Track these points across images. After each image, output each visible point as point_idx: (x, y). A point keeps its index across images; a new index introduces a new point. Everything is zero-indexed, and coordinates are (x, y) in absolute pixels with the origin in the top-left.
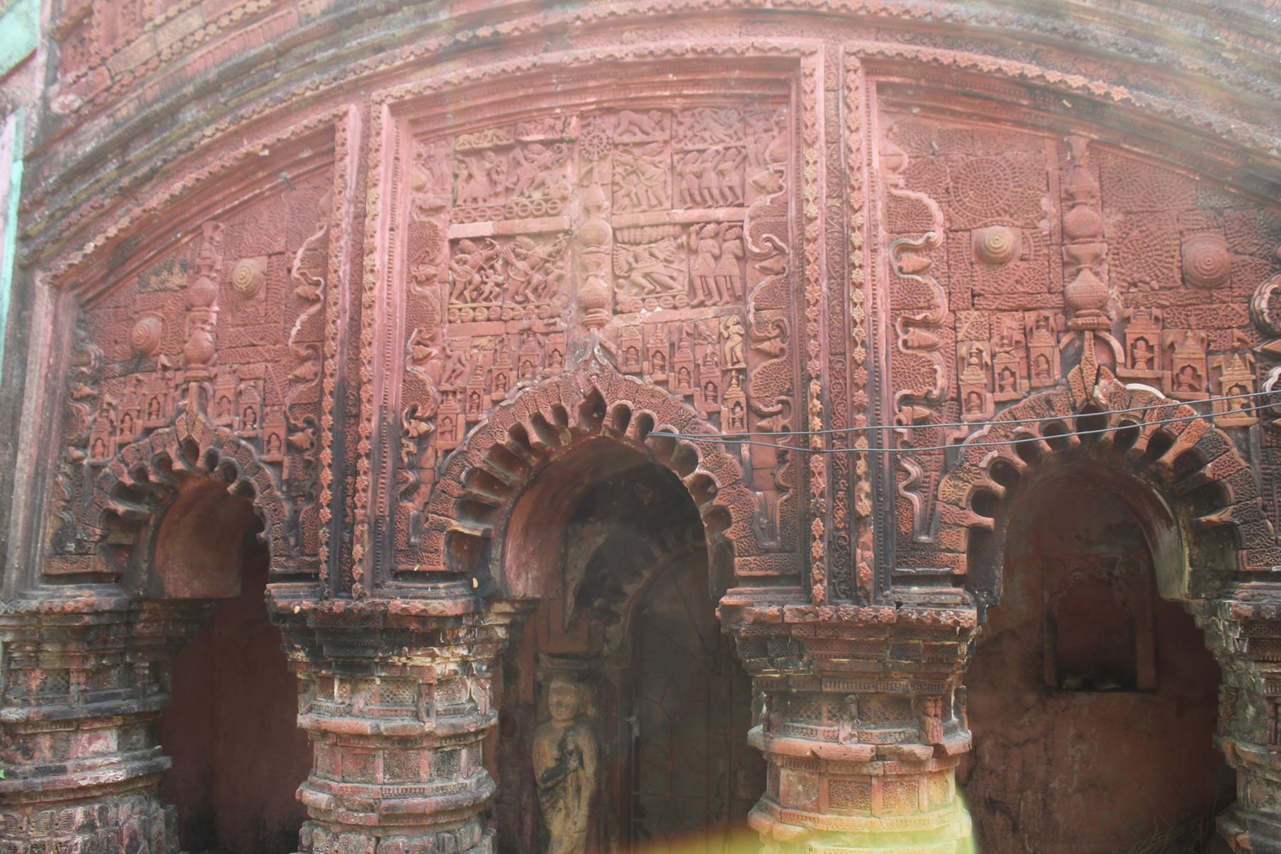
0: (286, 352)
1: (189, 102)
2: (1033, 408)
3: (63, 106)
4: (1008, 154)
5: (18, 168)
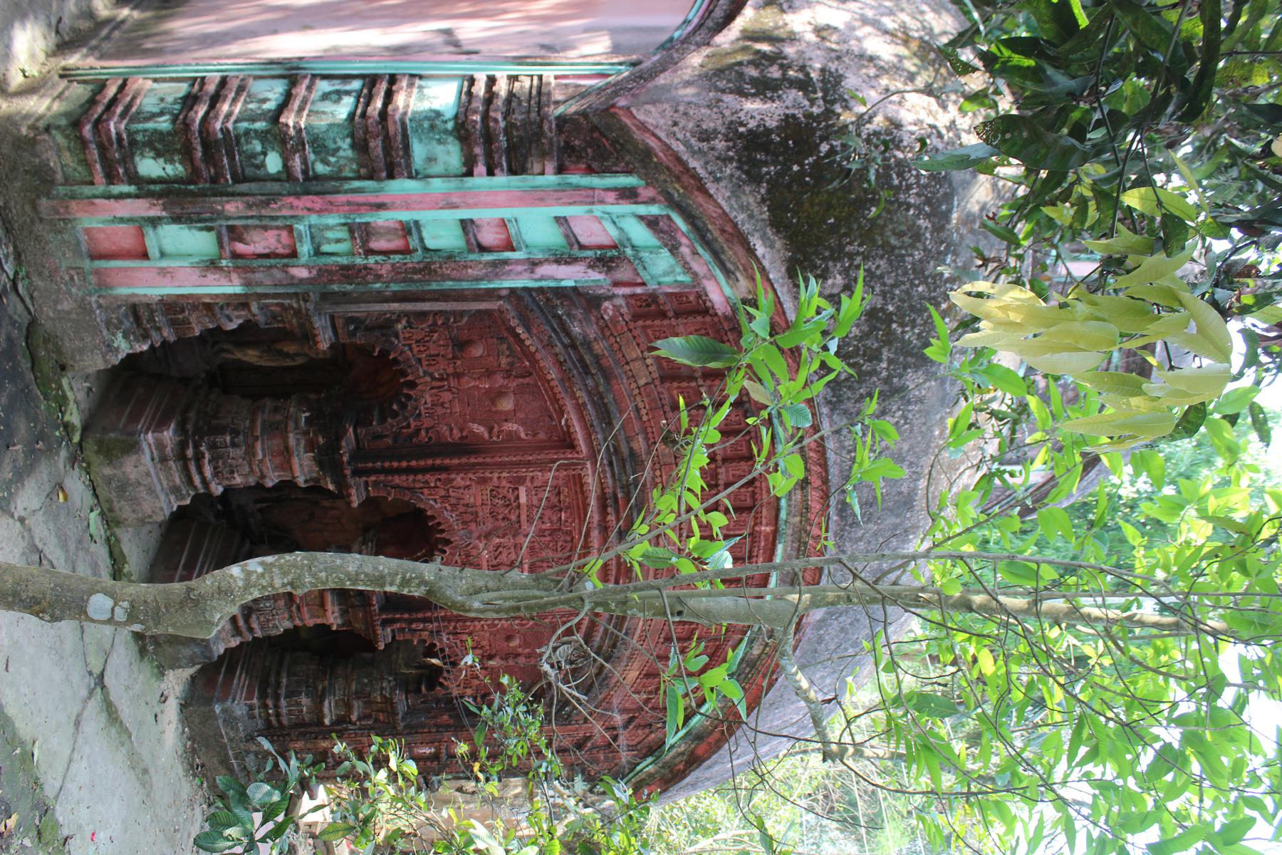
0: (466, 421)
3: (606, 308)
5: (570, 283)
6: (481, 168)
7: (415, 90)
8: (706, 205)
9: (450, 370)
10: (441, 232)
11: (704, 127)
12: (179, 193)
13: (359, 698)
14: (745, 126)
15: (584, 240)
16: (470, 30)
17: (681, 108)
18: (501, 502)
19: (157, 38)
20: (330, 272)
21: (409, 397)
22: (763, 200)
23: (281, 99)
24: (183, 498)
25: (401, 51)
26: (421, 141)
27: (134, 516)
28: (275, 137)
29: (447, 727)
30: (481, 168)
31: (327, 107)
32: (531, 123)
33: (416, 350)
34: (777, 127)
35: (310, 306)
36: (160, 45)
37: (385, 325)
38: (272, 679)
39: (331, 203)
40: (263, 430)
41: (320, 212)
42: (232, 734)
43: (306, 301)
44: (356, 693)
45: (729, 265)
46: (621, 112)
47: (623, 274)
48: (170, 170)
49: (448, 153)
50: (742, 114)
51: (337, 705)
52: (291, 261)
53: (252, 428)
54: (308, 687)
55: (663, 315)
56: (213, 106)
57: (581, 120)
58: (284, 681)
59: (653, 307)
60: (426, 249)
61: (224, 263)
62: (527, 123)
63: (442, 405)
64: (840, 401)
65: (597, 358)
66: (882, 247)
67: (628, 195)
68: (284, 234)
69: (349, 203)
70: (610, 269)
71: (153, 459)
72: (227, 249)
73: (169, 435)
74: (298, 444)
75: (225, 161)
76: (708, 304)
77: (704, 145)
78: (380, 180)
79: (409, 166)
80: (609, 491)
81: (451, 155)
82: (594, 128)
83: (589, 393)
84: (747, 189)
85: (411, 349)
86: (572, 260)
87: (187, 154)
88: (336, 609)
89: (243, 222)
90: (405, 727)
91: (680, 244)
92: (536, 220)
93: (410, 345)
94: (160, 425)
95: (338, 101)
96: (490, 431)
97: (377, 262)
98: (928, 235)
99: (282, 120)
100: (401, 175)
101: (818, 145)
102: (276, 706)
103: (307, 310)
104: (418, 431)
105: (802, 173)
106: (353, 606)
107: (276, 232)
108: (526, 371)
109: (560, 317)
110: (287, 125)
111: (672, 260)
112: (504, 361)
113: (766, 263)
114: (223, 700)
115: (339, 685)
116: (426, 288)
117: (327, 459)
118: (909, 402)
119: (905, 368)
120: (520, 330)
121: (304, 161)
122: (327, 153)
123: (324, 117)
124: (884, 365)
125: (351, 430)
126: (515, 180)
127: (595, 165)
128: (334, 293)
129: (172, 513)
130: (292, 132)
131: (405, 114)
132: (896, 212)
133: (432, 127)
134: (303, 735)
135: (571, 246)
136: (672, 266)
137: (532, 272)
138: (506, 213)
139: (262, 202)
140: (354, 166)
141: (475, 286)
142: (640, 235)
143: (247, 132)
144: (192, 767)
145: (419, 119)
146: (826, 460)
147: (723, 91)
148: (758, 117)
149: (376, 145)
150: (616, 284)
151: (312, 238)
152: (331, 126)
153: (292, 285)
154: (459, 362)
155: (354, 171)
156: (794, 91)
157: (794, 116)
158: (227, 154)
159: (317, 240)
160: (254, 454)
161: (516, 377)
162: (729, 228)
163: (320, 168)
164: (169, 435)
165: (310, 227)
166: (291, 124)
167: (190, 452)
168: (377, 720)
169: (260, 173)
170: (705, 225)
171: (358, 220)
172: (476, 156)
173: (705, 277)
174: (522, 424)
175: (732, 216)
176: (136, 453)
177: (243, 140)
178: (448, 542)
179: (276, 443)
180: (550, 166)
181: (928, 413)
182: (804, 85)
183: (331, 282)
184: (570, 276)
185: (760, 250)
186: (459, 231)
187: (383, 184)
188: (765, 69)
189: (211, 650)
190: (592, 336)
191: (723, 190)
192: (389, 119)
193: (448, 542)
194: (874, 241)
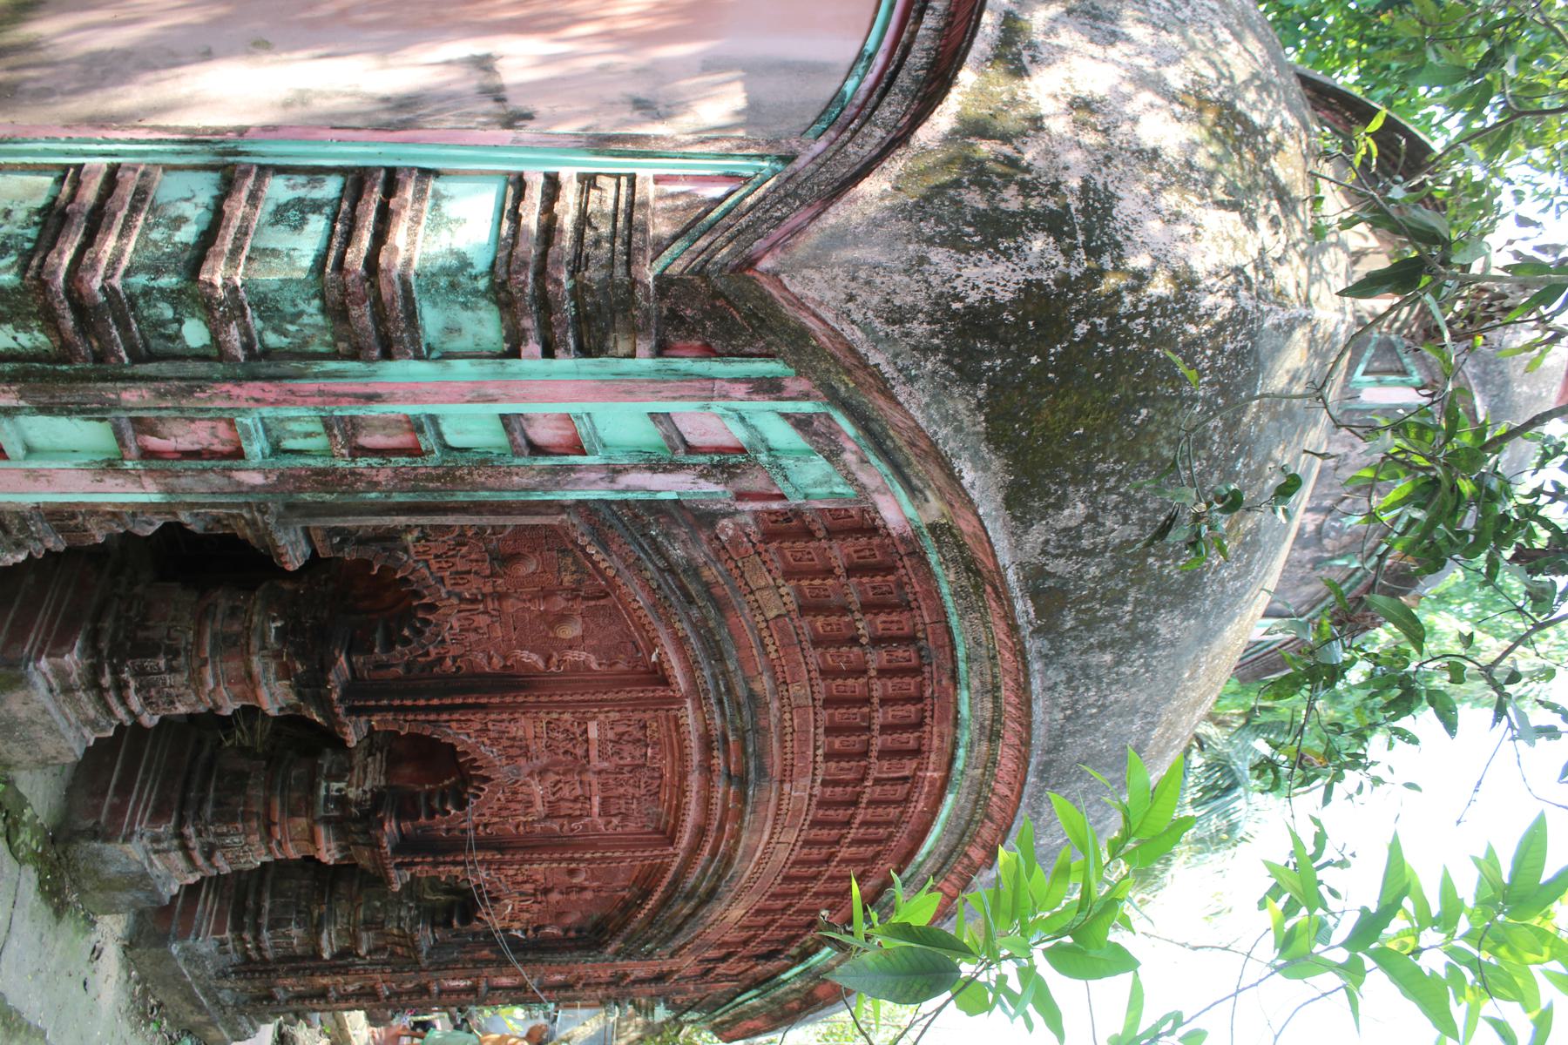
6: (532, 347)
7: (428, 204)
8: (889, 412)
9: (488, 589)
10: (471, 426)
11: (897, 302)
12: (43, 376)
13: (368, 930)
14: (961, 300)
15: (693, 439)
16: (519, 59)
17: (862, 274)
18: (561, 736)
19: (12, 60)
20: (297, 478)
21: (427, 622)
22: (980, 406)
23: (208, 217)
24: (103, 729)
25: (403, 113)
26: (435, 304)
27: (29, 758)
28: (194, 298)
29: (488, 962)
30: (532, 347)
31: (279, 238)
32: (615, 287)
33: (434, 565)
34: (1012, 301)
35: (271, 520)
36: (16, 75)
37: (390, 538)
38: (250, 903)
39: (293, 393)
40: (215, 648)
41: (276, 403)
42: (197, 972)
43: (263, 513)
44: (365, 922)
45: (915, 481)
46: (763, 279)
47: (753, 482)
48: (25, 340)
49: (480, 321)
50: (958, 283)
51: (338, 935)
52: (236, 463)
53: (198, 643)
54: (299, 912)
55: (810, 535)
56: (89, 240)
57: (698, 281)
58: (267, 905)
59: (794, 523)
60: (447, 448)
61: (129, 465)
62: (608, 284)
63: (476, 630)
64: (1058, 654)
65: (707, 586)
66: (1149, 462)
67: (769, 387)
68: (222, 427)
69: (321, 393)
70: (732, 476)
71: (51, 691)
72: (133, 446)
73: (73, 660)
74: (266, 670)
75: (115, 332)
76: (878, 522)
77: (896, 330)
78: (370, 360)
79: (415, 341)
80: (716, 733)
81: (485, 326)
82: (717, 294)
83: (693, 625)
84: (956, 391)
85: (428, 567)
86: (678, 467)
87: (50, 320)
88: (333, 845)
89: (153, 414)
90: (431, 964)
91: (843, 450)
92: (617, 416)
93: (426, 561)
94: (59, 643)
95: (298, 227)
96: (547, 660)
97: (370, 466)
98: (1216, 438)
99: (204, 276)
100: (404, 355)
101: (1073, 326)
102: (256, 938)
103: (267, 524)
104: (441, 660)
105: (1044, 367)
106: (355, 843)
107: (210, 424)
108: (599, 595)
109: (653, 539)
110: (212, 285)
111: (828, 467)
112: (567, 579)
113: (975, 495)
114: (183, 936)
115: (342, 909)
116: (447, 499)
117: (311, 685)
118: (1156, 648)
119: (1156, 609)
120: (591, 550)
121: (246, 331)
122: (284, 318)
123: (275, 262)
124: (1129, 608)
125: (343, 658)
126: (588, 364)
127: (717, 344)
128: (306, 505)
129: (88, 749)
130: (221, 293)
131: (408, 262)
132: (1176, 412)
133: (453, 286)
134: (295, 971)
135: (674, 450)
136: (828, 475)
137: (613, 481)
138: (573, 408)
139: (183, 390)
140: (328, 338)
141: (523, 497)
142: (782, 435)
143: (147, 292)
144: (144, 1015)
145: (430, 279)
146: (1029, 714)
147: (930, 241)
148: (983, 287)
149: (362, 315)
150: (741, 496)
151: (267, 430)
152: (286, 282)
153: (240, 493)
154: (500, 581)
155: (328, 344)
156: (1041, 236)
157: (1039, 282)
158: (116, 321)
159: (274, 434)
160: (202, 682)
161: (586, 598)
162: (923, 444)
163: (272, 339)
164: (73, 660)
165: (262, 419)
166: (218, 281)
167: (106, 680)
168: (393, 954)
169: (176, 347)
170: (884, 429)
171: (337, 413)
172: (525, 330)
173: (877, 490)
174: (594, 651)
175: (930, 432)
176: (24, 688)
177: (141, 302)
178: (487, 779)
179: (234, 665)
180: (644, 347)
181: (1179, 655)
182: (1055, 224)
183: (300, 490)
184: (668, 486)
185: (968, 476)
186: (499, 425)
187: (374, 367)
188: (988, 196)
189: (160, 895)
190: (701, 560)
191: (919, 395)
192: (382, 276)
193: (487, 779)
194: (1139, 454)
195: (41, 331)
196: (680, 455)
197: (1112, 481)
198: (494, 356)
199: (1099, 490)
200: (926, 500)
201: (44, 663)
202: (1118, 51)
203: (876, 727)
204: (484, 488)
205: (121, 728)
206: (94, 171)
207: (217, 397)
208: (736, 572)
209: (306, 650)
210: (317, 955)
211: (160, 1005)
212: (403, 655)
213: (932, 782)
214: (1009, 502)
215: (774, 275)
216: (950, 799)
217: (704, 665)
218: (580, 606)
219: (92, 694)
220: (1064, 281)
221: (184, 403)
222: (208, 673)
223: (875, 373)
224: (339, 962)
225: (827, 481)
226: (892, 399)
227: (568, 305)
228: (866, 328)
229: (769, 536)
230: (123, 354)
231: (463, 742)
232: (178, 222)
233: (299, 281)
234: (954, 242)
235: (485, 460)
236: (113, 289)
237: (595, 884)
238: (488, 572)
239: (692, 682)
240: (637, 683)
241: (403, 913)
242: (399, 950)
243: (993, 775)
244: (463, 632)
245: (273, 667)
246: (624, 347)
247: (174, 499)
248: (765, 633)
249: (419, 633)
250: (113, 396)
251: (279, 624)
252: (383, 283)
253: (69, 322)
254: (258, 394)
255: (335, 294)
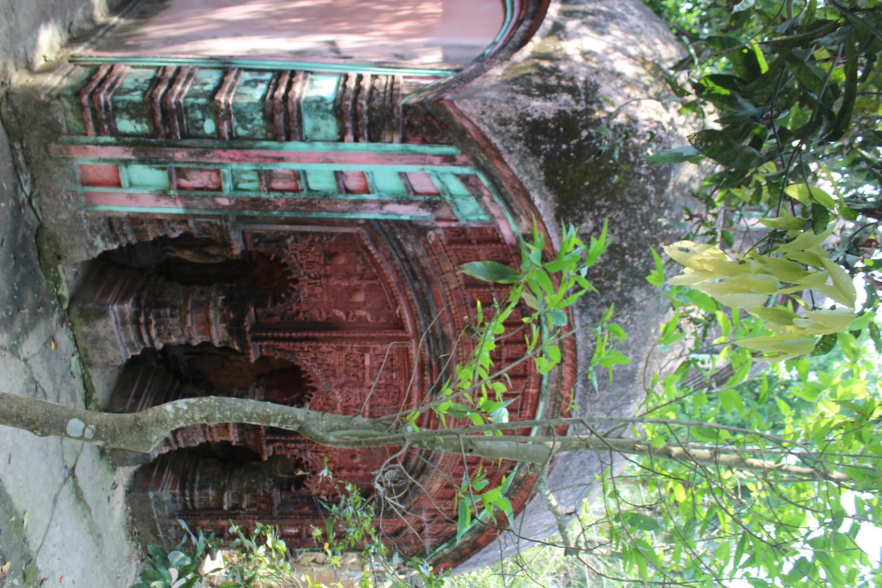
1: (493, 56)
2: (765, 474)
4: (839, 75)
6: (350, 137)
9: (322, 272)
10: (320, 179)
11: (503, 116)
12: (144, 144)
13: (247, 493)
15: (417, 188)
17: (488, 103)
18: (352, 364)
19: (136, 38)
20: (243, 202)
21: (293, 289)
22: (541, 167)
23: (217, 83)
24: (135, 350)
26: (310, 116)
27: (101, 361)
28: (211, 109)
29: (307, 515)
30: (350, 137)
31: (248, 90)
32: (386, 108)
33: (299, 257)
34: (553, 119)
35: (229, 225)
37: (279, 240)
38: (190, 477)
39: (247, 156)
41: (239, 161)
42: (160, 513)
45: (516, 211)
46: (447, 104)
47: (443, 213)
49: (328, 125)
51: (233, 497)
55: (469, 242)
58: (198, 478)
59: (462, 237)
60: (309, 190)
62: (382, 107)
63: (315, 296)
65: (423, 269)
66: (621, 203)
67: (449, 159)
68: (214, 175)
69: (259, 156)
71: (116, 323)
72: (175, 183)
76: (500, 236)
77: (503, 129)
78: (280, 141)
79: (301, 133)
80: (426, 360)
81: (330, 127)
83: (416, 293)
84: (531, 159)
85: (296, 257)
86: (409, 202)
88: (236, 431)
89: (186, 166)
90: (279, 514)
92: (385, 174)
94: (123, 299)
95: (255, 86)
96: (347, 315)
97: (276, 197)
99: (217, 98)
100: (295, 139)
102: (191, 495)
103: (227, 227)
104: (298, 312)
105: (568, 150)
109: (398, 240)
110: (220, 102)
111: (477, 205)
113: (541, 210)
114: (155, 488)
117: (235, 328)
118: (635, 309)
119: (633, 286)
120: (371, 248)
121: (230, 126)
124: (619, 283)
125: (252, 310)
126: (373, 146)
127: (428, 138)
128: (245, 217)
130: (223, 106)
133: (318, 108)
134: (209, 516)
135: (409, 192)
136: (477, 209)
137: (381, 208)
138: (365, 168)
140: (264, 131)
142: (456, 187)
143: (193, 105)
145: (309, 103)
147: (517, 92)
148: (540, 111)
149: (279, 118)
150: (438, 219)
151: (233, 178)
152: (249, 104)
153: (217, 209)
154: (328, 268)
159: (236, 180)
160: (185, 323)
161: (367, 279)
162: (517, 186)
163: (241, 132)
166: (223, 100)
167: (142, 319)
168: (260, 508)
169: (200, 133)
173: (499, 217)
177: (189, 110)
178: (314, 389)
179: (201, 316)
180: (397, 138)
182: (572, 91)
183: (244, 209)
184: (406, 213)
185: (537, 201)
187: (282, 145)
188: (546, 79)
193: (314, 389)
195: (147, 123)
196: (412, 196)
197: (604, 211)
198: (333, 141)
199: (599, 214)
200: (521, 221)
201: (115, 307)
202: (608, 38)
203: (503, 358)
204: (324, 210)
205: (145, 350)
206: (171, 68)
207: (213, 158)
208: (436, 262)
209: (235, 307)
210: (221, 508)
211: (139, 533)
212: (280, 309)
213: (533, 395)
214: (557, 218)
215: (451, 102)
216: (541, 405)
217: (421, 317)
218: (365, 284)
219: (135, 327)
220: (575, 112)
221: (201, 159)
222: (189, 317)
223: (495, 149)
224: (232, 512)
225: (476, 213)
226: (501, 160)
227: (365, 117)
228: (490, 127)
229: (451, 242)
230: (178, 134)
231: (305, 365)
232: (205, 84)
233: (255, 103)
234: (528, 93)
235: (326, 196)
236: (179, 103)
237: (365, 466)
238: (322, 263)
239: (415, 330)
240: (390, 329)
241: (266, 484)
242: (263, 506)
243: (562, 386)
244: (312, 297)
245: (219, 317)
246: (388, 138)
247: (189, 212)
248: (449, 298)
249: (289, 295)
250: (171, 155)
251: (223, 297)
252: (290, 103)
253: (159, 118)
254: (232, 156)
255: (269, 110)
